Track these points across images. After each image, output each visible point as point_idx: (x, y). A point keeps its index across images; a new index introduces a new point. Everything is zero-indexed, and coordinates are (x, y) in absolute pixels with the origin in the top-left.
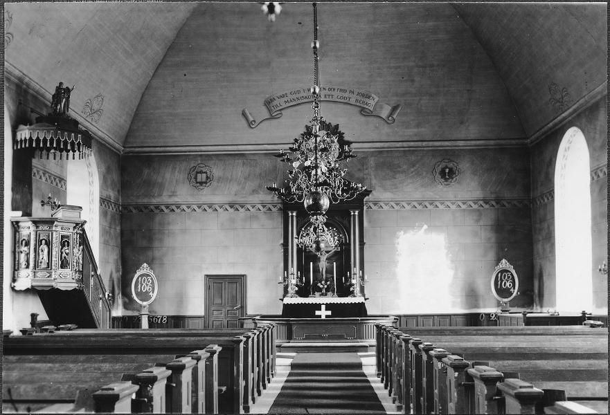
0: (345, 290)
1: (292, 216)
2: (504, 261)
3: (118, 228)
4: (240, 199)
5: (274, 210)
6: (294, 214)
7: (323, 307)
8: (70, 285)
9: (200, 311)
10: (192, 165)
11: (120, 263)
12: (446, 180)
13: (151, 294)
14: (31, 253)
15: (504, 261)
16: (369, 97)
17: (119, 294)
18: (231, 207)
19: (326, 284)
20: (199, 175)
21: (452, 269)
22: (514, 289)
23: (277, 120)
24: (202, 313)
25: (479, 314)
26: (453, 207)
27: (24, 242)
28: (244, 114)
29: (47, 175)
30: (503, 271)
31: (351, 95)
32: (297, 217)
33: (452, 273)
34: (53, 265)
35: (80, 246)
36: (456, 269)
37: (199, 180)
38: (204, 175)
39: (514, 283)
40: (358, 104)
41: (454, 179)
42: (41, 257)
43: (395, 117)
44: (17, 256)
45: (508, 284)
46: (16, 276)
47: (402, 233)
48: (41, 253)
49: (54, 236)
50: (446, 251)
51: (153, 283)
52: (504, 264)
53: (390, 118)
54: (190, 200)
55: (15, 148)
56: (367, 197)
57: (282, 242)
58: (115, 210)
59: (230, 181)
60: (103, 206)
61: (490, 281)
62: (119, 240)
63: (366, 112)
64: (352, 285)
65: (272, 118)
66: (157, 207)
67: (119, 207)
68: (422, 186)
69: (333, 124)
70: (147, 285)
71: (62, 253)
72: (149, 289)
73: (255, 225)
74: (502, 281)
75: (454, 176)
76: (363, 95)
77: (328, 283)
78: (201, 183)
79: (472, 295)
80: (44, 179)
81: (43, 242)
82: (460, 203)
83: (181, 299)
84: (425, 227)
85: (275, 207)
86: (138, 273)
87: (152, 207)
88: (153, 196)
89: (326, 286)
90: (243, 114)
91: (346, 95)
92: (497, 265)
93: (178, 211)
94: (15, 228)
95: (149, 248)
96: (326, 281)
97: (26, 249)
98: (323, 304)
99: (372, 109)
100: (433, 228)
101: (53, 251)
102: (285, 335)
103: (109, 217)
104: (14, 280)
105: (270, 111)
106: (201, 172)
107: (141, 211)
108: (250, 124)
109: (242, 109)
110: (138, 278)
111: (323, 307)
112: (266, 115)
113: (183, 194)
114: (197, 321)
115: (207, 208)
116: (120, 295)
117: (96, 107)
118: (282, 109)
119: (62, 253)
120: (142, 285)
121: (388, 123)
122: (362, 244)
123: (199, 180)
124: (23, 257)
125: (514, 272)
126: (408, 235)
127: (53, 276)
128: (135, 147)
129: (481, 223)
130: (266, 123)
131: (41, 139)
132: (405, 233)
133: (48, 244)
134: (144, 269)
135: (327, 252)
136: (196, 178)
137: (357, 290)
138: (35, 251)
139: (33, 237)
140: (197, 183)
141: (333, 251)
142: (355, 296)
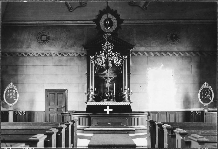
0: (120, 98)
2: (206, 83)
4: (65, 50)
7: (108, 107)
10: (39, 31)
12: (173, 41)
13: (15, 99)
15: (206, 83)
20: (43, 37)
26: (177, 55)
30: (205, 89)
38: (45, 37)
43: (147, 7)
45: (208, 96)
51: (16, 93)
52: (206, 85)
54: (38, 50)
57: (86, 72)
64: (123, 95)
69: (114, 9)
70: (13, 94)
72: (14, 97)
73: (72, 64)
74: (204, 94)
77: (111, 94)
83: (32, 102)
84: (162, 65)
85: (83, 54)
86: (7, 88)
87: (17, 53)
88: (18, 48)
89: (110, 96)
95: (16, 75)
98: (108, 105)
106: (44, 35)
108: (69, 9)
111: (108, 107)
113: (34, 47)
114: (41, 114)
115: (47, 54)
125: (211, 89)
130: (79, 9)
134: (11, 85)
135: (110, 78)
140: (41, 41)
141: (114, 77)
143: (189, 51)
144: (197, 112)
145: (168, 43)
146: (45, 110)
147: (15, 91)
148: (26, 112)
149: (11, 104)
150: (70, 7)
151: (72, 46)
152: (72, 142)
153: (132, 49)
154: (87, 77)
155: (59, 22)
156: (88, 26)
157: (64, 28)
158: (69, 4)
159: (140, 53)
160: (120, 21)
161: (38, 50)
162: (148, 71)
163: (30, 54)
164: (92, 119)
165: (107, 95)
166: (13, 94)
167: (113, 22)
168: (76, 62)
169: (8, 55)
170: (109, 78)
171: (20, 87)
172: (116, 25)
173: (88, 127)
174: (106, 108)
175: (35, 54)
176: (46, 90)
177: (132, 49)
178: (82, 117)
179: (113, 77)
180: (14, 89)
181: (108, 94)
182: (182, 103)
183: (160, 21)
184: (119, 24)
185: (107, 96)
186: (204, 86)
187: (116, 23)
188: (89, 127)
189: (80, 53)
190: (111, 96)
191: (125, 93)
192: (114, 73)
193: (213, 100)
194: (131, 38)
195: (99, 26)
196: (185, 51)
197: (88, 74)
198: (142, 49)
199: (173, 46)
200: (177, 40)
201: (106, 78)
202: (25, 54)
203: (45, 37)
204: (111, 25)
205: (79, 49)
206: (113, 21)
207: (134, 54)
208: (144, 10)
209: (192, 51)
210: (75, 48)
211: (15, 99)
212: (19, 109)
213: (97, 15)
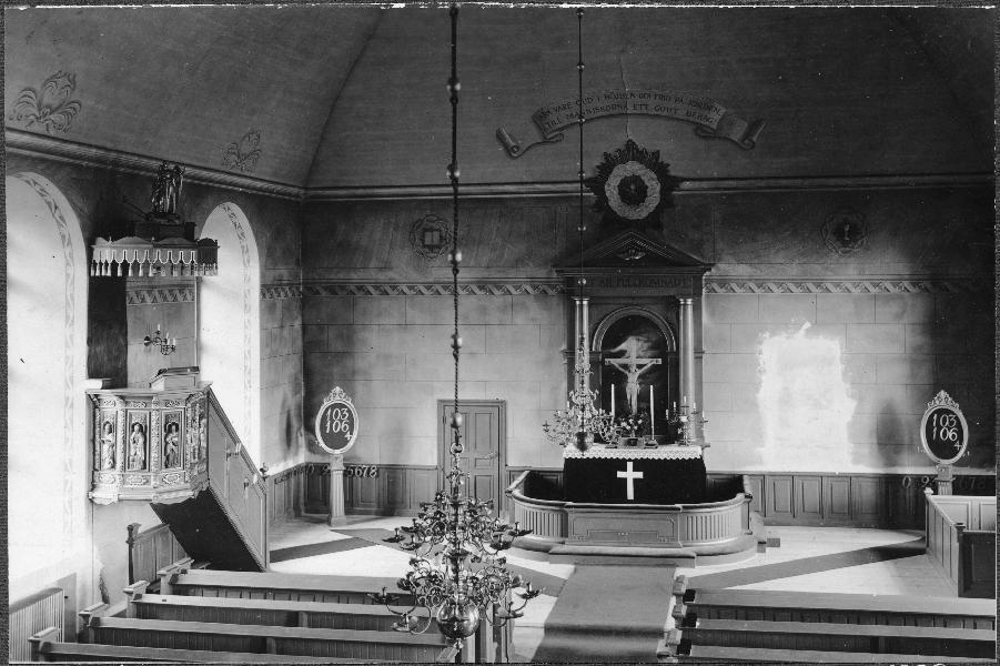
0: (670, 434)
1: (581, 306)
2: (943, 394)
3: (298, 324)
4: (494, 274)
5: (550, 292)
6: (585, 303)
7: (630, 465)
8: (181, 494)
9: (431, 459)
10: (416, 217)
11: (301, 378)
12: (845, 244)
13: (348, 436)
14: (118, 444)
15: (943, 394)
16: (709, 108)
17: (299, 429)
18: (481, 288)
19: (636, 424)
20: (428, 234)
21: (852, 397)
22: (961, 444)
23: (554, 146)
24: (435, 463)
25: (901, 476)
26: (856, 291)
27: (107, 427)
28: (500, 137)
29: (156, 292)
30: (940, 412)
31: (679, 105)
32: (590, 305)
33: (851, 405)
34: (152, 464)
35: (201, 418)
36: (861, 400)
37: (428, 241)
38: (436, 234)
39: (960, 432)
40: (691, 119)
41: (859, 242)
42: (132, 453)
43: (754, 139)
44: (98, 448)
45: (950, 434)
46: (96, 479)
47: (767, 335)
48: (132, 445)
49: (153, 418)
50: (844, 366)
51: (351, 418)
52: (943, 399)
53: (746, 141)
54: (414, 276)
55: (92, 274)
56: (708, 273)
57: (564, 347)
58: (290, 295)
59: (479, 244)
60: (268, 295)
61: (920, 420)
62: (299, 343)
63: (705, 131)
64: (680, 425)
65: (546, 141)
66: (360, 288)
67: (298, 288)
68: (802, 254)
69: (650, 149)
70: (341, 421)
71: (167, 443)
72: (345, 428)
73: (520, 319)
74: (939, 428)
75: (858, 237)
76: (698, 105)
77: (640, 422)
78: (432, 248)
79: (889, 438)
80: (149, 300)
81: (136, 428)
82: (867, 284)
83: (399, 435)
84: (807, 325)
85: (553, 287)
86: (326, 404)
87: (353, 288)
88: (355, 269)
89: (636, 428)
90: (497, 136)
91: (672, 104)
92: (931, 399)
93: (393, 293)
94: (94, 403)
95: (346, 354)
96: (637, 418)
97: (109, 437)
98: (630, 460)
99: (715, 127)
100: (819, 326)
101: (152, 441)
102: (556, 527)
103: (279, 312)
104: (93, 487)
105: (541, 129)
106: (432, 230)
107: (335, 293)
108: (509, 150)
109: (496, 128)
110: (327, 410)
111: (630, 465)
112: (535, 136)
113: (403, 268)
114: (425, 475)
115: (441, 290)
116: (302, 431)
117: (246, 148)
118: (563, 129)
119: (167, 443)
120: (332, 421)
121: (745, 149)
122: (699, 353)
123: (428, 241)
124: (106, 450)
125: (960, 415)
126: (777, 338)
127: (153, 483)
128: (323, 188)
129: (905, 321)
130: (540, 149)
131: (130, 263)
132: (773, 334)
133: (143, 430)
134: (337, 395)
135: (640, 367)
136: (423, 241)
137: (690, 432)
138: (124, 442)
139: (120, 420)
140: (425, 246)
141: (649, 365)
142: (682, 444)
143: (896, 277)
144: (925, 480)
145: (826, 250)
146: (435, 463)
147: (349, 411)
148: (379, 468)
149: (337, 452)
150: (513, 144)
151: (518, 263)
152: (497, 638)
153: (710, 270)
154: (566, 361)
155: (478, 189)
156: (566, 198)
157: (494, 206)
158: (507, 136)
159: (734, 286)
160: (669, 183)
161: (414, 276)
162: (760, 343)
163: (390, 291)
164: (571, 517)
165: (629, 424)
166: (341, 421)
167: (647, 187)
168: (531, 313)
169: (324, 294)
170: (633, 369)
171: (359, 387)
172: (657, 195)
173: (561, 540)
174: (624, 469)
175: (406, 290)
176: (440, 401)
177: (710, 270)
178: (547, 512)
179: (649, 362)
180: (346, 407)
181: (631, 421)
182: (875, 447)
183: (800, 181)
184: (665, 192)
185: (628, 428)
186: (937, 402)
187: (658, 188)
188: (563, 543)
189: (546, 287)
190: (639, 426)
191: (684, 419)
192: (650, 348)
193: (966, 452)
194: (705, 237)
195: (603, 198)
196: (885, 277)
197: (570, 354)
198: (742, 270)
199: (842, 260)
200: (856, 241)
201: (626, 367)
202: (376, 288)
203: (436, 234)
204: (642, 192)
205: (542, 273)
206: (647, 183)
207: (715, 286)
208: (745, 149)
209: (907, 277)
210: (529, 269)
211: (348, 436)
212: (359, 459)
213: (598, 167)
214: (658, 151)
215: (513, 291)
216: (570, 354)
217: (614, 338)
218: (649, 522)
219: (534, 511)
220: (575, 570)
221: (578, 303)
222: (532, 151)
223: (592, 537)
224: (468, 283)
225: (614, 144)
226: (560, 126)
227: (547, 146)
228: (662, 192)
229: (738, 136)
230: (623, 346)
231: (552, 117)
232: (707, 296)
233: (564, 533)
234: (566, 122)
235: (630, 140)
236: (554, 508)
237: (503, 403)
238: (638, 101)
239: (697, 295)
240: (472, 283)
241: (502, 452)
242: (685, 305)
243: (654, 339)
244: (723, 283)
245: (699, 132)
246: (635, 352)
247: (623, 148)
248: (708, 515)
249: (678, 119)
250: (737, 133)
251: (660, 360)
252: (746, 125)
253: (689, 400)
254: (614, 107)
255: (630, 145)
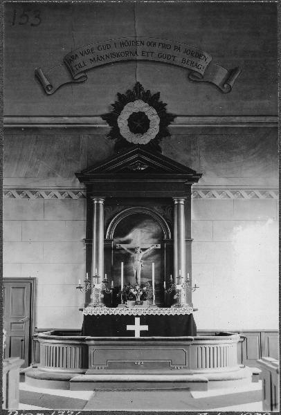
5: (75, 197)
7: (137, 320)
28: (38, 77)
31: (176, 53)
32: (105, 205)
40: (185, 66)
57: (84, 237)
63: (195, 77)
65: (74, 82)
77: (145, 288)
89: (141, 293)
91: (170, 52)
98: (137, 316)
99: (203, 73)
108: (45, 89)
111: (137, 320)
118: (85, 72)
122: (189, 240)
130: (68, 88)
135: (144, 250)
137: (183, 300)
150: (47, 83)
151: (50, 174)
158: (44, 77)
164: (91, 351)
172: (157, 127)
173: (81, 371)
174: (133, 323)
187: (158, 121)
188: (84, 373)
198: (222, 181)
201: (133, 250)
213: (113, 105)
214: (159, 93)
215: (44, 195)
216: (89, 269)
217: (122, 231)
218: (161, 353)
219: (61, 346)
220: (96, 395)
221: (96, 202)
222: (61, 90)
223: (112, 366)
224: (11, 189)
225: (125, 87)
226: (86, 68)
227: (76, 87)
228: (161, 125)
229: (220, 81)
230: (130, 236)
231: (78, 61)
232: (194, 201)
233: (85, 364)
234: (90, 65)
235: (138, 83)
236: (76, 342)
237: (33, 279)
238: (147, 48)
239: (187, 193)
240: (13, 189)
241: (33, 318)
242: (179, 204)
243: (154, 231)
244: (206, 191)
245: (190, 77)
246: (141, 239)
247: (132, 89)
248: (211, 347)
249: (175, 65)
250: (219, 79)
251: (159, 245)
252: (226, 72)
253: (181, 271)
254: (126, 53)
255: (138, 86)
